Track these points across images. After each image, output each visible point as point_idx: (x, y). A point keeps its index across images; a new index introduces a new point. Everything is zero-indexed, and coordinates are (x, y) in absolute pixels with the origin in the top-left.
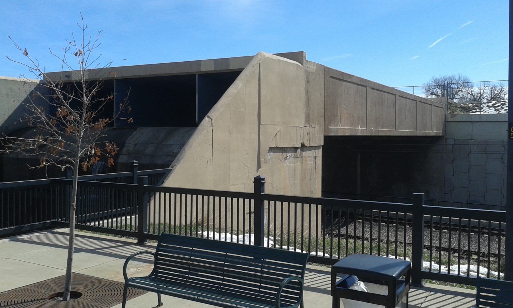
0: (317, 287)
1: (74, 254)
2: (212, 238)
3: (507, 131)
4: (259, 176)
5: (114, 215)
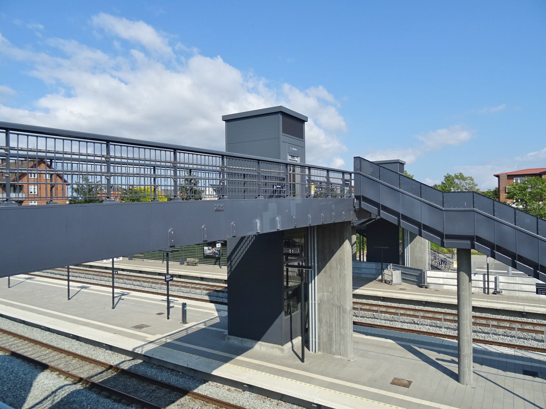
1: (497, 290)
4: (402, 164)
5: (445, 235)
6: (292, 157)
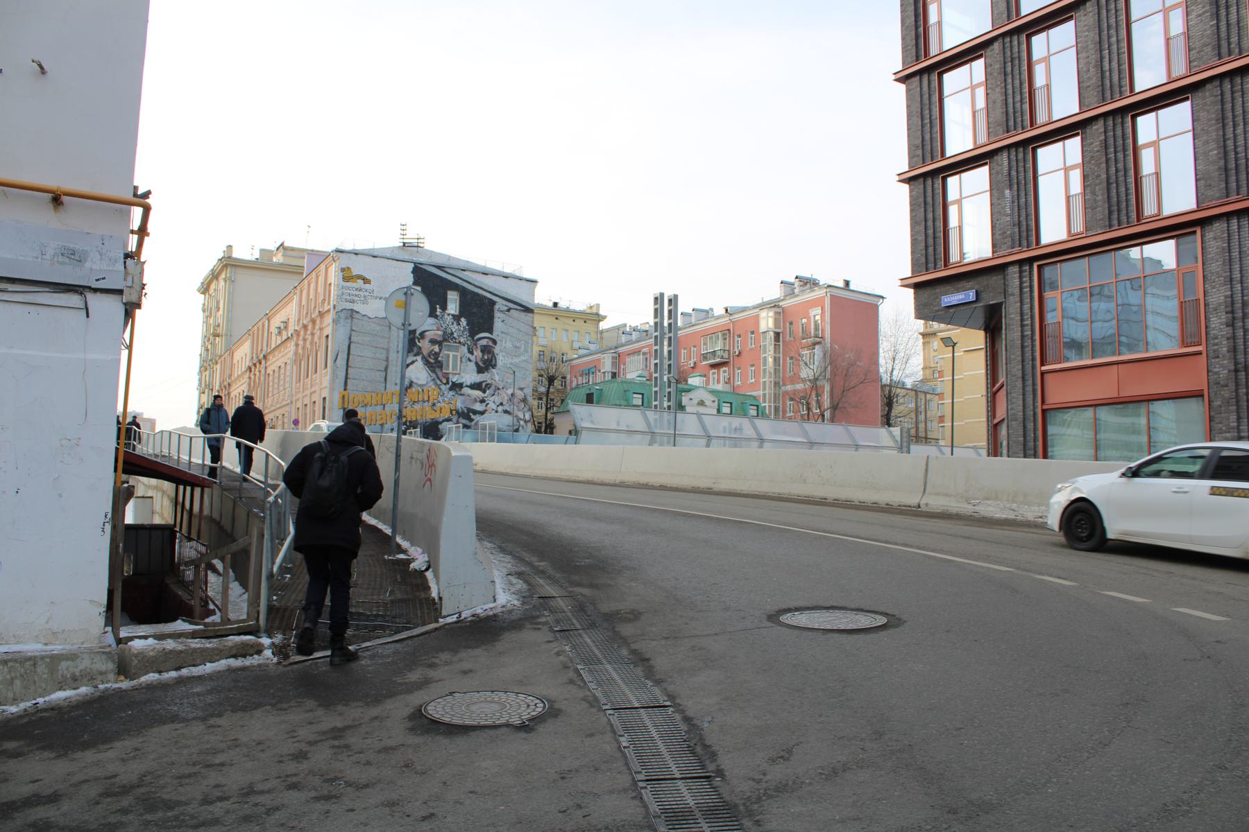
0: (60, 292)
2: (962, 255)
3: (847, 283)
4: (148, 235)
6: (174, 500)
